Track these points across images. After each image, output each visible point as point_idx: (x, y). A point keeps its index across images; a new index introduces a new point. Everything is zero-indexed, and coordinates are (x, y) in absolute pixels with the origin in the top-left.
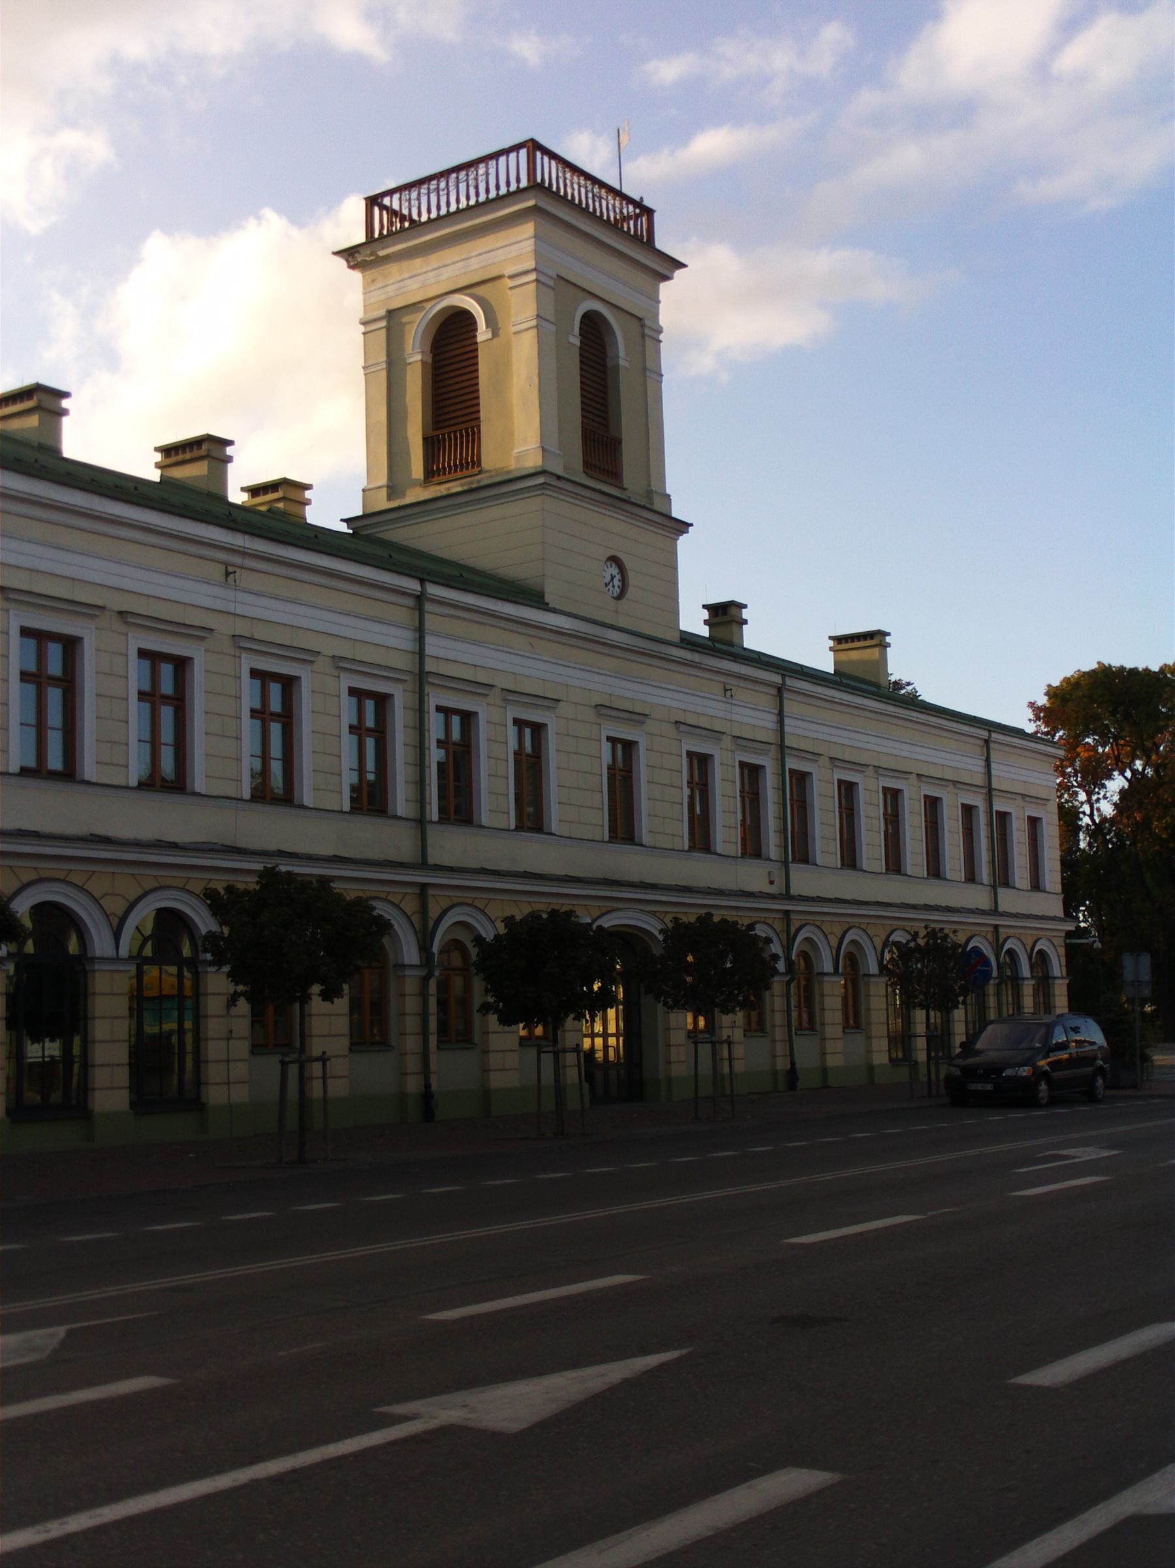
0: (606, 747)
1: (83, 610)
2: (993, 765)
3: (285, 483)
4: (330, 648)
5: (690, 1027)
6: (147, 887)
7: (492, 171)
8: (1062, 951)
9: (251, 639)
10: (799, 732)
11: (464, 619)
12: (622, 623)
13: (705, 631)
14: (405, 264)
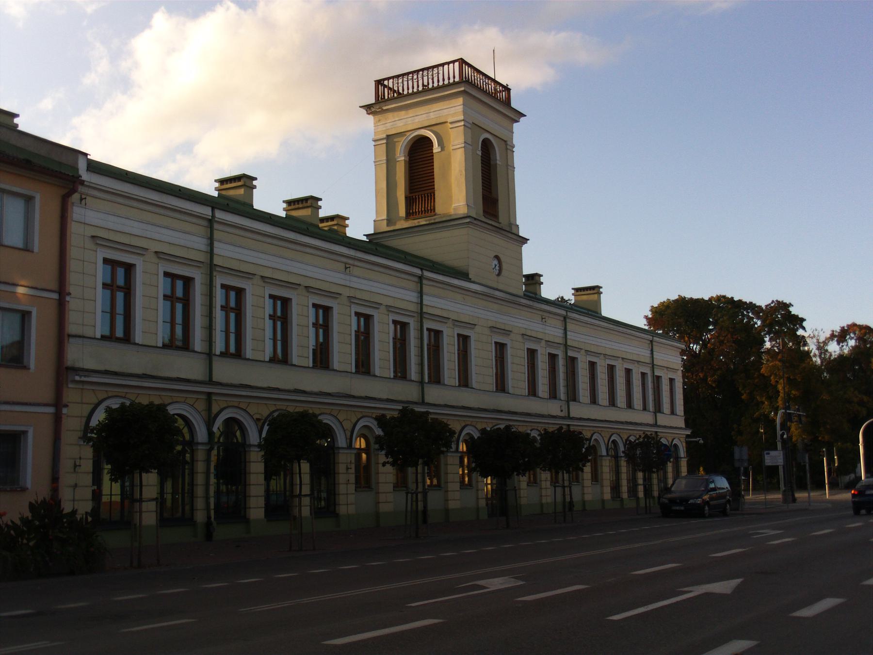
3: (338, 217)
4: (454, 316)
7: (441, 72)
8: (684, 444)
12: (501, 287)
13: (646, 328)
14: (396, 114)
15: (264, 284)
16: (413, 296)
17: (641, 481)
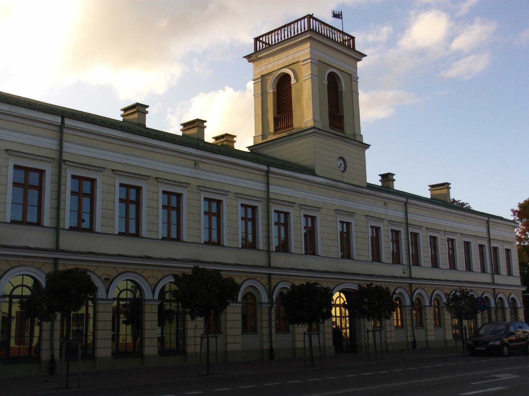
0: (339, 225)
1: (85, 167)
2: (490, 230)
3: (227, 135)
4: (299, 202)
5: (396, 324)
6: (165, 275)
7: (296, 26)
8: (521, 298)
9: (204, 187)
10: (414, 219)
11: (286, 180)
12: (345, 180)
13: (380, 184)
14: (267, 59)
16: (262, 187)
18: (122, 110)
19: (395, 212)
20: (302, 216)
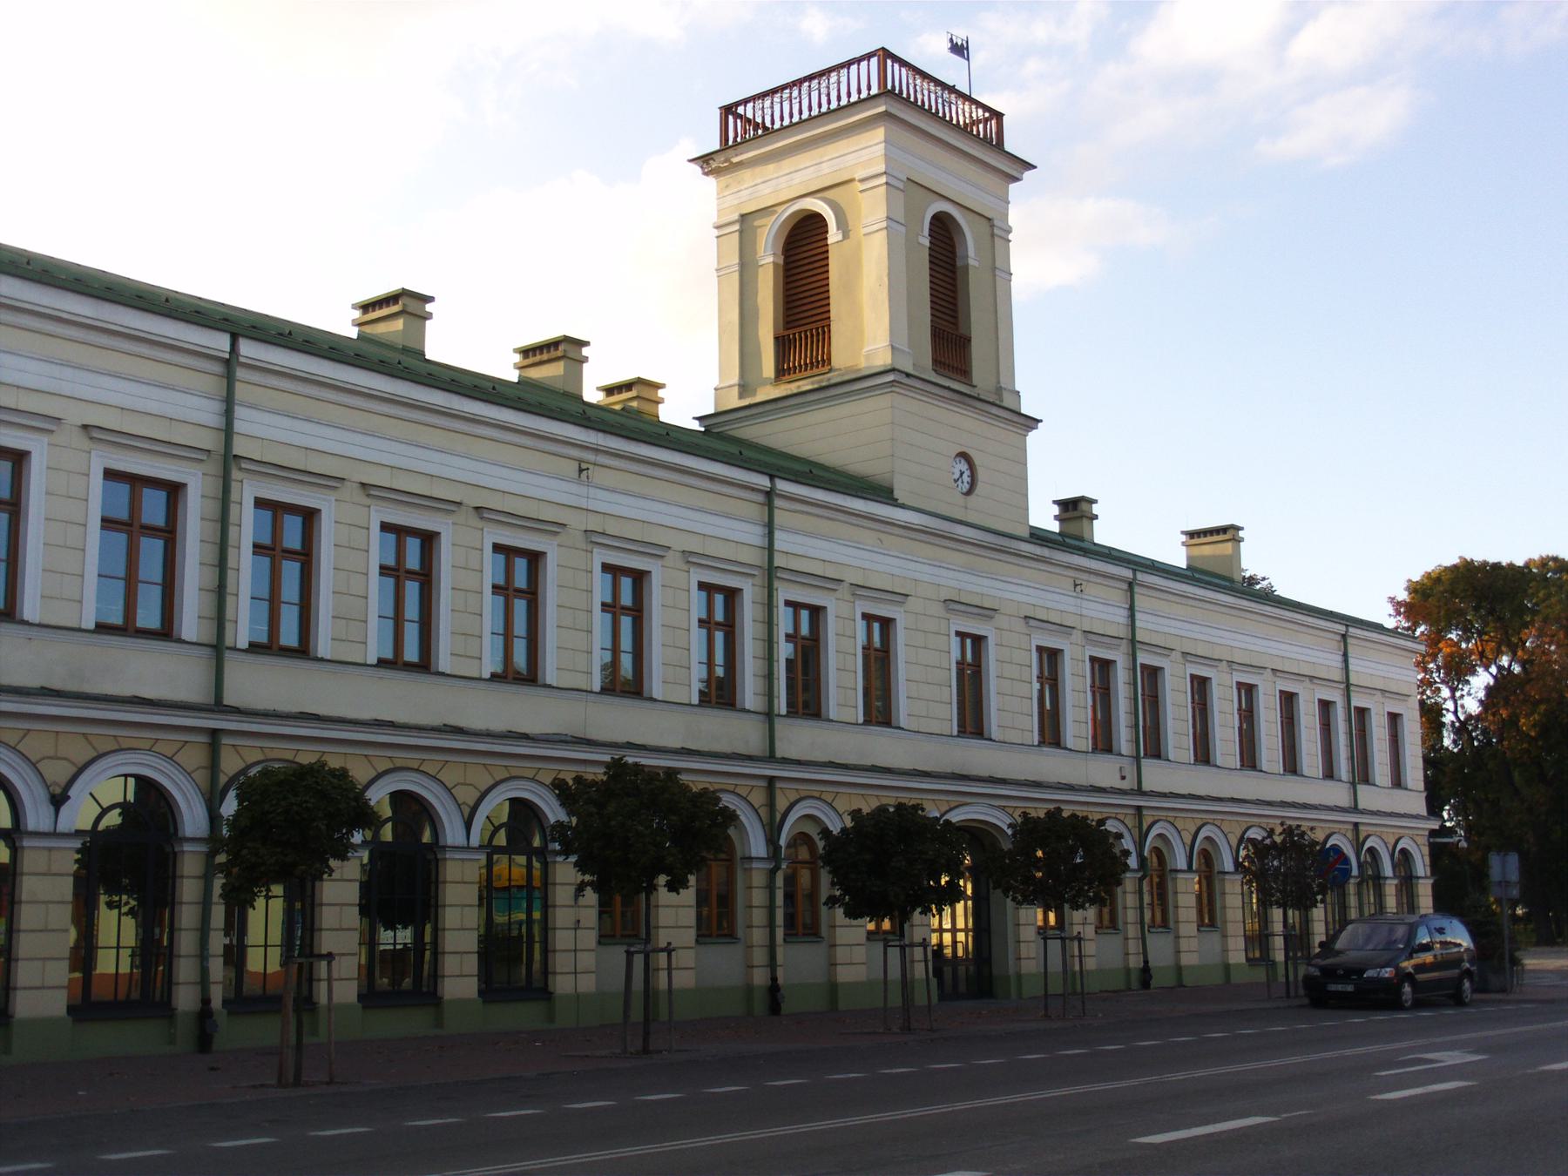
2: (1351, 660)
4: (851, 577)
5: (1040, 923)
7: (844, 79)
8: (1426, 850)
11: (803, 512)
13: (1055, 527)
14: (758, 170)
15: (368, 501)
16: (752, 534)
17: (1278, 927)
18: (355, 307)
19: (1101, 607)
20: (859, 617)
